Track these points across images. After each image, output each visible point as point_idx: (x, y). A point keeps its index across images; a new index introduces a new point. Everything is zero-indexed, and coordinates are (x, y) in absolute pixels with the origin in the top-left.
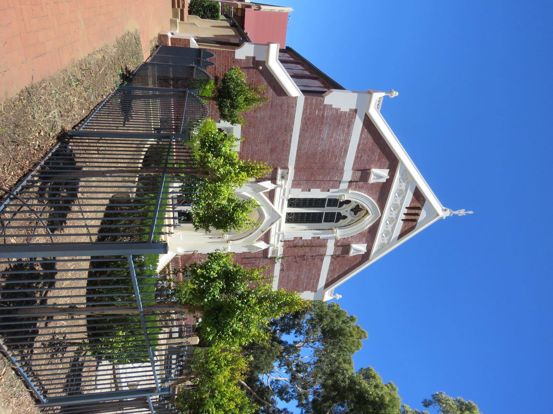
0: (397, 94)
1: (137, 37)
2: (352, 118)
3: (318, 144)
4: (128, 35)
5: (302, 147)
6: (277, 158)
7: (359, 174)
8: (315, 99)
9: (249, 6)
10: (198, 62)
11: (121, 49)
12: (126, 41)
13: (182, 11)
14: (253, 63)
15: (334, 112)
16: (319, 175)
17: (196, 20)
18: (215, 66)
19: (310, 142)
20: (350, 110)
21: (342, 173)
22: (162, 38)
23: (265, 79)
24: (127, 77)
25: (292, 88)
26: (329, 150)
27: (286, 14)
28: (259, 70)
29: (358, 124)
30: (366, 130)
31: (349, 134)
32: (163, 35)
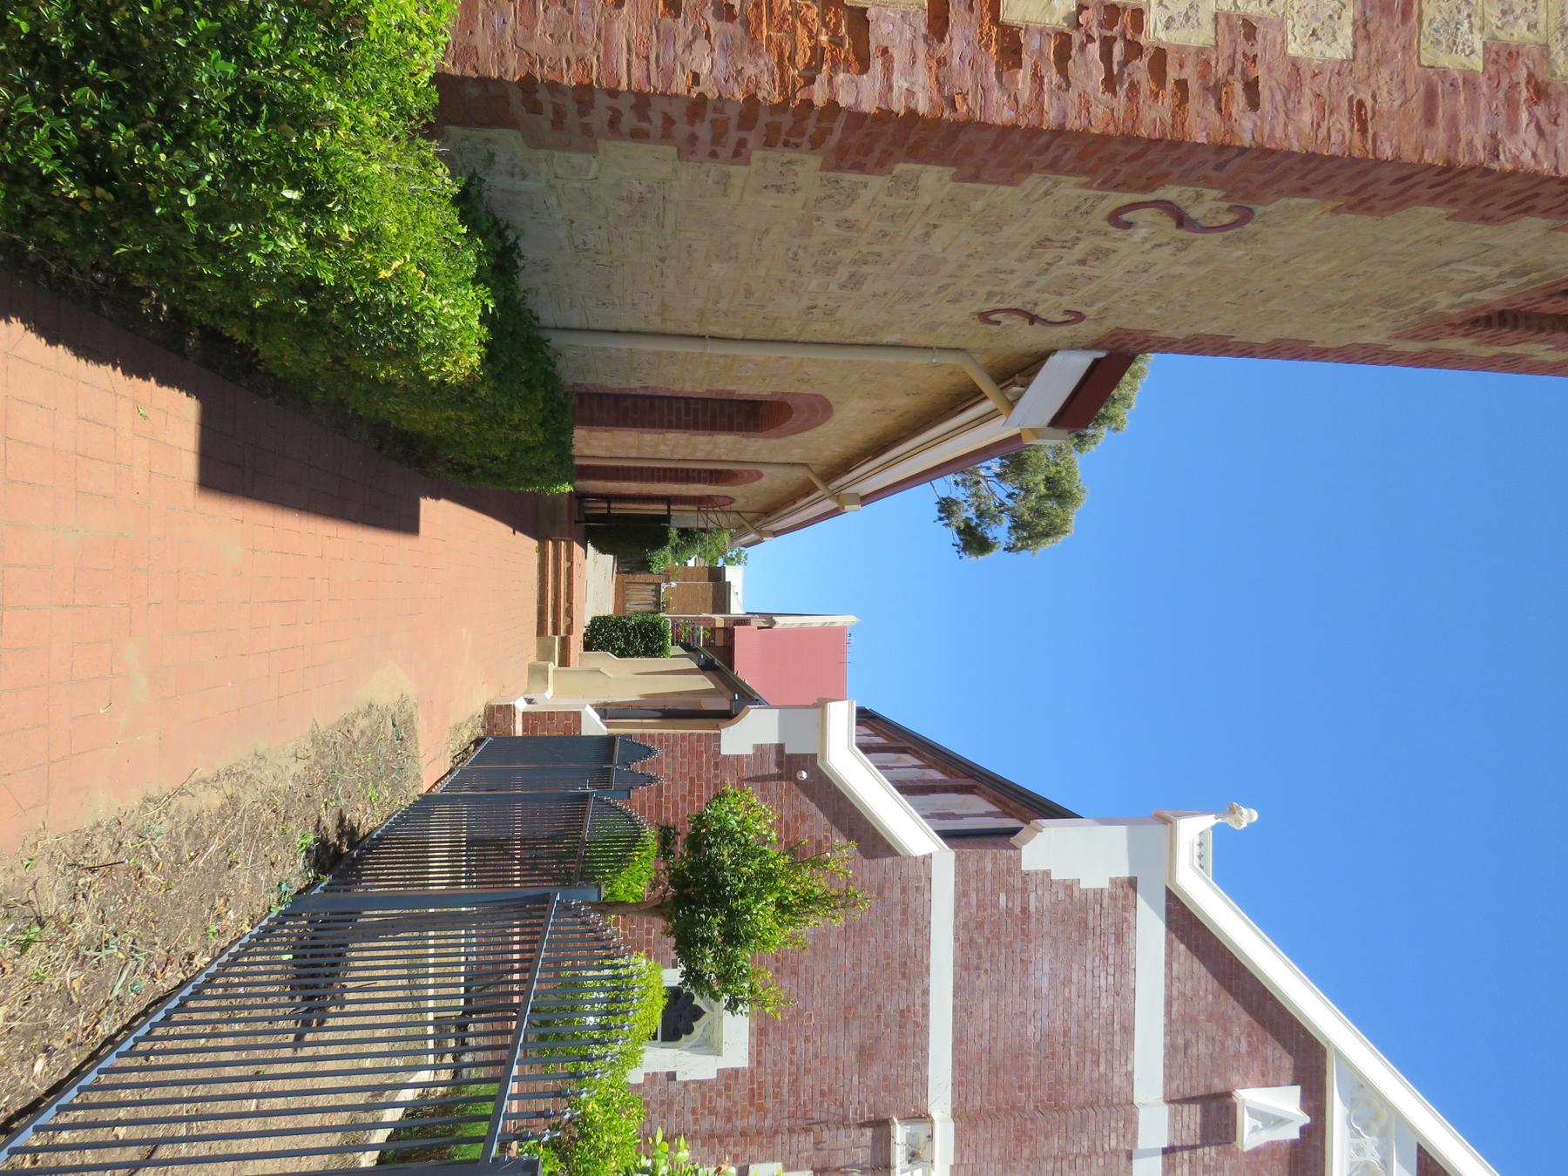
0: (1255, 816)
1: (404, 716)
2: (1124, 909)
3: (1023, 1013)
4: (367, 714)
5: (971, 1030)
6: (885, 1078)
7: (1193, 1115)
8: (988, 858)
9: (743, 622)
10: (603, 778)
11: (329, 761)
12: (356, 734)
13: (565, 644)
14: (779, 764)
15: (1061, 896)
16: (1046, 1136)
17: (606, 662)
18: (659, 789)
19: (994, 1008)
20: (1113, 881)
21: (1130, 1120)
22: (497, 714)
23: (820, 806)
24: (340, 857)
25: (906, 826)
26: (1065, 1034)
27: (842, 630)
28: (798, 783)
29: (1150, 928)
30: (1182, 947)
31: (1124, 966)
32: (500, 707)
